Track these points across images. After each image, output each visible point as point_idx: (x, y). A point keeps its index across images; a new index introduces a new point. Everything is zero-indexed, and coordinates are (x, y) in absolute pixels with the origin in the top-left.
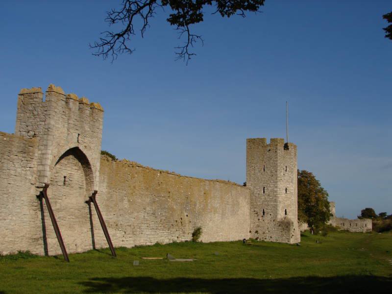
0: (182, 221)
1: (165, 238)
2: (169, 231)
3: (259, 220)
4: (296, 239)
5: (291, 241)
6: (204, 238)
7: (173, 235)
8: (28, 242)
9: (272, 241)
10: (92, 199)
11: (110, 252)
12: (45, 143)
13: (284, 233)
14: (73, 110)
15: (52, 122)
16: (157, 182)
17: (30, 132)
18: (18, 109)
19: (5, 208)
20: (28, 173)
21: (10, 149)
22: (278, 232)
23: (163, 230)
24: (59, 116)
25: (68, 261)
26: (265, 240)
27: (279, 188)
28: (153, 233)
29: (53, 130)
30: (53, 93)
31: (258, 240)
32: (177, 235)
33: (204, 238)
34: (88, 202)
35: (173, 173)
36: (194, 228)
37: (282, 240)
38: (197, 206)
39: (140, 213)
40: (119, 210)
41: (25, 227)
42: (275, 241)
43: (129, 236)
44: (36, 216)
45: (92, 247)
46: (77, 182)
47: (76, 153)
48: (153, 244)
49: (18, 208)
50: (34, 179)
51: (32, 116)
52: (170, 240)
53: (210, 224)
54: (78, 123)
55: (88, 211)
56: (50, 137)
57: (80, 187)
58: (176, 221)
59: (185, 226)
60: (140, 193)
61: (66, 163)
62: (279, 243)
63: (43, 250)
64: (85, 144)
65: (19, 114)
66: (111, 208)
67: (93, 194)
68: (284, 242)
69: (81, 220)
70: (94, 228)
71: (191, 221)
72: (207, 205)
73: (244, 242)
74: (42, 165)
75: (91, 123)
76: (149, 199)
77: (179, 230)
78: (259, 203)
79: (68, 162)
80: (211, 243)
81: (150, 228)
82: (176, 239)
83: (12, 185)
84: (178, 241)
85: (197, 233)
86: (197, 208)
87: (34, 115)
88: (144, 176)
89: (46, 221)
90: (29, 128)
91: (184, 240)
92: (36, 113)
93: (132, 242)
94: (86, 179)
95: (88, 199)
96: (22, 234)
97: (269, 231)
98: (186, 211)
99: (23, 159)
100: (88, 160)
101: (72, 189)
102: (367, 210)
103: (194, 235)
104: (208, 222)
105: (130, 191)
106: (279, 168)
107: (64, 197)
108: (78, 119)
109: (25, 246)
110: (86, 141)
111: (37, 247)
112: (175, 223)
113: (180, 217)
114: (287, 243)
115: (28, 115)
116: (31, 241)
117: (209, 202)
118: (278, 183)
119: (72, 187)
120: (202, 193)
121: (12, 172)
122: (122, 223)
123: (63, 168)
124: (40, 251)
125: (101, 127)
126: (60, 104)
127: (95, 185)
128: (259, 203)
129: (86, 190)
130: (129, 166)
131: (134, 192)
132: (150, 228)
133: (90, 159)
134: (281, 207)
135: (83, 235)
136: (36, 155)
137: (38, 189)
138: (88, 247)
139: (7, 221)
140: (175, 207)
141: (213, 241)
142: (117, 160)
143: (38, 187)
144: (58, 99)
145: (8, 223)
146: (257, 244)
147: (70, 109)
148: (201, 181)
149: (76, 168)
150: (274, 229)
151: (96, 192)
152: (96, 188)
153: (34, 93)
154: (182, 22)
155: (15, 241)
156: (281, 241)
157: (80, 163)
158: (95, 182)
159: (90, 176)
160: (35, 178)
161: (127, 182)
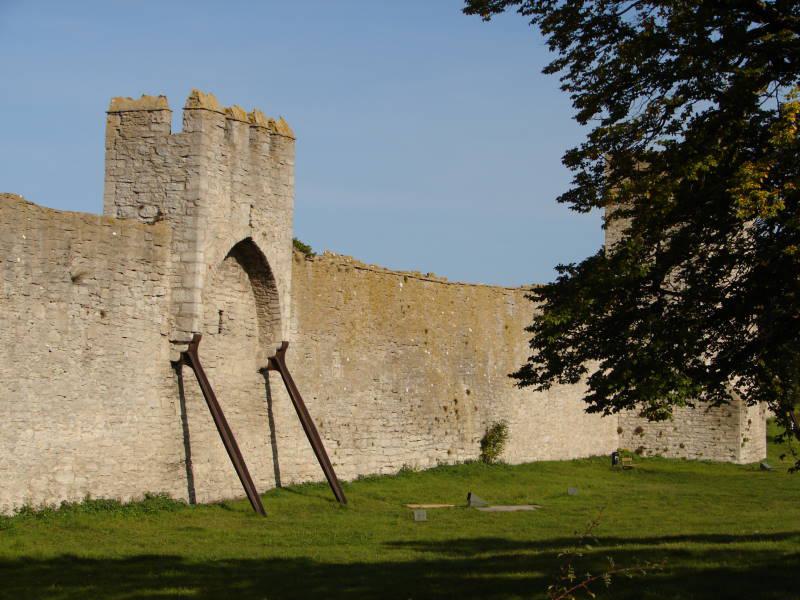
0: (459, 406)
1: (421, 454)
2: (431, 437)
4: (755, 451)
5: (742, 457)
6: (512, 453)
7: (439, 446)
8: (162, 472)
9: (684, 459)
10: (277, 362)
11: (329, 494)
12: (188, 235)
13: (719, 433)
14: (239, 148)
15: (204, 185)
16: (399, 304)
17: (147, 207)
18: (108, 149)
19: (120, 394)
20: (156, 309)
21: (123, 256)
22: (703, 430)
23: (417, 434)
24: (215, 166)
25: (263, 513)
26: (665, 455)
28: (396, 442)
29: (204, 201)
30: (203, 112)
31: (645, 454)
32: (448, 447)
33: (512, 453)
34: (263, 371)
35: (427, 278)
36: (484, 426)
37: (715, 453)
38: (491, 363)
39: (367, 392)
40: (325, 385)
41: (155, 437)
42: (694, 457)
43: (349, 451)
44: (172, 411)
45: (274, 482)
46: (242, 323)
47: (248, 256)
48: (395, 471)
49: (141, 393)
50: (166, 323)
51: (149, 170)
52: (431, 458)
53: (521, 412)
54: (249, 178)
55: (263, 392)
56: (201, 221)
57: (248, 332)
58: (445, 408)
59: (465, 421)
60: (365, 340)
61: (222, 278)
62: (708, 463)
63: (186, 490)
64: (263, 229)
65: (113, 163)
66: (309, 381)
67: (278, 350)
68: (721, 459)
69: (250, 415)
70: (277, 434)
71: (478, 405)
72: (512, 359)
73: (614, 462)
74: (185, 288)
75: (273, 173)
76: (384, 353)
77: (451, 433)
79: (225, 276)
80: (524, 467)
81: (389, 429)
82: (445, 456)
83: (128, 341)
84: (451, 463)
85: (493, 438)
86: (489, 370)
87: (155, 167)
88: (371, 294)
89: (189, 422)
90: (144, 198)
91: (462, 459)
92: (158, 161)
93: (353, 468)
94: (260, 314)
95: (265, 363)
96: (150, 456)
97: (676, 429)
98: (464, 379)
99: (146, 278)
100: (268, 268)
101: (234, 340)
103: (485, 443)
104: (516, 407)
105: (345, 336)
107: (220, 361)
108: (249, 168)
109: (155, 483)
110: (265, 220)
111: (176, 483)
112: (442, 415)
113: (452, 398)
114: (729, 463)
115: (137, 165)
116: (166, 470)
117: (516, 349)
119: (234, 335)
120: (500, 329)
121: (129, 311)
122: (331, 418)
123: (217, 291)
124: (180, 493)
125: (292, 181)
126: (215, 138)
127: (283, 327)
129: (260, 341)
130: (339, 270)
131: (353, 337)
132: (389, 429)
133: (272, 264)
135: (256, 452)
136: (169, 264)
137: (176, 347)
138: (266, 482)
139: (123, 425)
140: (439, 371)
141: (531, 459)
142: (314, 255)
143: (175, 342)
144: (212, 127)
145: (127, 430)
146: (646, 466)
147: (233, 146)
148: (495, 291)
149: (238, 287)
150: (689, 422)
151: (285, 345)
152: (286, 336)
153: (149, 111)
154: (614, 32)
155: (139, 471)
156: (711, 458)
157: (247, 275)
158: (283, 321)
159: (271, 305)
160: (169, 320)
161: (337, 312)
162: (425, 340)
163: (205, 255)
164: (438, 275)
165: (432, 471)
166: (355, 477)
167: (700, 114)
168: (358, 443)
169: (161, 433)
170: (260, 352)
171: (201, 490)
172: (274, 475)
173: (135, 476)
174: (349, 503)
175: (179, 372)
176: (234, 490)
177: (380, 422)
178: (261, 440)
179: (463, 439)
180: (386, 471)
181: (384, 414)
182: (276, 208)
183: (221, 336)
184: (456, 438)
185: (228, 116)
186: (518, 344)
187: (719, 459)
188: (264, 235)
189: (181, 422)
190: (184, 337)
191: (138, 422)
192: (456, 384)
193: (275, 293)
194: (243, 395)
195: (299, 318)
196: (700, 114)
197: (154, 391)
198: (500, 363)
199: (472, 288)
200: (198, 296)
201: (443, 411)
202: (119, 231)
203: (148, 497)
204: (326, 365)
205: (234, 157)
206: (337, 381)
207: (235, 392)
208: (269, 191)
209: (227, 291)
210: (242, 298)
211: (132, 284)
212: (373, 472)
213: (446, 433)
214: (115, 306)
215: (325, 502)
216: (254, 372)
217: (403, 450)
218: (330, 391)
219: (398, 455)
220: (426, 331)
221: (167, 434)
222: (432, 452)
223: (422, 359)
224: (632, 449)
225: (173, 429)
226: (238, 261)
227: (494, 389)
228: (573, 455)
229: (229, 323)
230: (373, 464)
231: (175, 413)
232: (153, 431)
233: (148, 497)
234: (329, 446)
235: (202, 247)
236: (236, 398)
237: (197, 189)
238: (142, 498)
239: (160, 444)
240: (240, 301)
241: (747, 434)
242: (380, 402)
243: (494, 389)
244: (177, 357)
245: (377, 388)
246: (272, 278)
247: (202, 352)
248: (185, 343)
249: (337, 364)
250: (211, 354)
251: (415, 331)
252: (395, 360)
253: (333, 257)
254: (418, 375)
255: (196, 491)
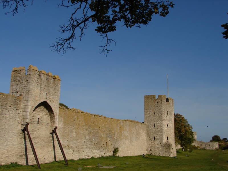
1: (87, 154)
2: (100, 150)
3: (152, 143)
6: (120, 154)
8: (17, 157)
9: (160, 156)
10: (54, 132)
11: (65, 163)
12: (27, 99)
14: (43, 80)
15: (31, 87)
16: (92, 121)
17: (18, 92)
19: (3, 137)
20: (17, 116)
21: (7, 103)
22: (163, 150)
23: (96, 150)
26: (156, 155)
27: (164, 124)
28: (90, 151)
30: (32, 70)
31: (152, 155)
32: (104, 152)
33: (120, 154)
37: (166, 155)
38: (116, 135)
39: (82, 140)
40: (70, 138)
42: (161, 155)
43: (77, 153)
45: (54, 160)
47: (45, 105)
49: (11, 137)
50: (20, 120)
52: (100, 155)
54: (46, 87)
55: (52, 138)
56: (30, 96)
57: (47, 124)
58: (104, 144)
59: (109, 147)
62: (164, 157)
63: (25, 162)
64: (50, 100)
73: (143, 156)
74: (25, 112)
76: (87, 131)
78: (152, 133)
80: (124, 157)
81: (88, 148)
82: (104, 154)
83: (7, 124)
84: (105, 156)
85: (116, 151)
87: (21, 83)
90: (18, 90)
91: (108, 155)
92: (21, 81)
93: (78, 157)
94: (51, 120)
95: (52, 131)
96: (13, 153)
97: (158, 150)
100: (52, 109)
101: (42, 125)
102: (215, 136)
103: (114, 152)
106: (163, 113)
107: (38, 130)
108: (46, 85)
109: (14, 160)
110: (51, 97)
111: (22, 160)
112: (103, 146)
113: (106, 142)
114: (169, 157)
117: (122, 132)
118: (163, 121)
119: (43, 125)
120: (119, 128)
121: (8, 116)
122: (72, 145)
123: (38, 113)
125: (59, 90)
126: (36, 76)
127: (56, 123)
128: (152, 133)
129: (51, 126)
130: (76, 112)
132: (88, 148)
133: (53, 108)
134: (165, 135)
135: (49, 153)
138: (51, 160)
141: (125, 155)
143: (22, 125)
145: (5, 146)
146: (152, 157)
147: (41, 79)
148: (118, 120)
149: (44, 113)
151: (56, 128)
152: (57, 125)
153: (21, 70)
155: (9, 157)
156: (165, 156)
157: (47, 111)
159: (53, 118)
160: (21, 119)
162: (99, 129)
163: (31, 104)
164: (104, 116)
165: (99, 158)
168: (79, 151)
169: (17, 147)
170: (50, 129)
171: (30, 161)
172: (54, 158)
173: (7, 158)
174: (69, 165)
175: (24, 133)
176: (35, 163)
177: (86, 147)
178: (50, 150)
179: (108, 151)
180: (87, 158)
181: (87, 145)
183: (38, 125)
184: (106, 151)
186: (123, 131)
187: (166, 156)
188: (50, 101)
189: (24, 145)
190: (24, 123)
191: (9, 144)
193: (54, 115)
194: (45, 139)
195: (63, 122)
197: (15, 136)
198: (119, 135)
199: (112, 119)
200: (28, 114)
201: (103, 145)
202: (6, 96)
203: (11, 163)
204: (71, 133)
208: (52, 91)
210: (46, 116)
212: (84, 158)
213: (104, 150)
214: (3, 115)
215: (63, 165)
216: (49, 133)
217: (92, 153)
218: (71, 139)
219: (91, 154)
220: (99, 127)
222: (100, 154)
223: (98, 133)
224: (149, 154)
225: (22, 146)
226: (45, 107)
228: (136, 155)
229: (41, 122)
230: (84, 156)
231: (22, 142)
232: (15, 147)
233: (11, 163)
235: (30, 102)
236: (43, 139)
237: (29, 88)
238: (10, 163)
240: (45, 116)
242: (86, 142)
243: (117, 140)
244: (23, 129)
245: (85, 139)
247: (29, 128)
248: (25, 125)
249: (74, 133)
250: (35, 129)
251: (96, 127)
252: (91, 133)
253: (74, 109)
254: (97, 136)
255: (29, 162)
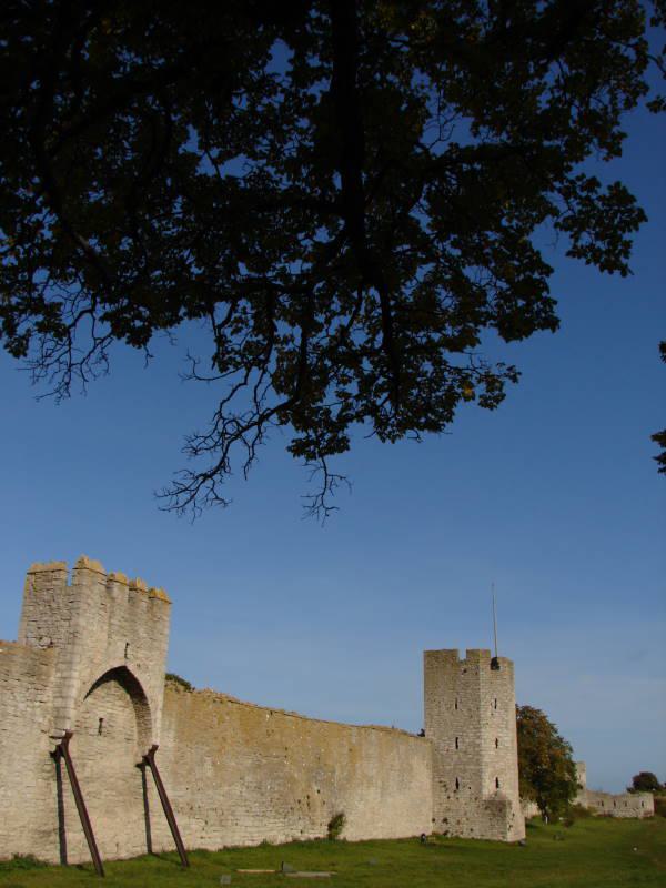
0: (310, 800)
1: (279, 833)
6: (349, 833)
10: (148, 760)
11: (179, 859)
15: (82, 622)
20: (38, 711)
28: (256, 823)
29: (82, 634)
31: (449, 835)
33: (349, 833)
34: (140, 766)
37: (492, 835)
39: (233, 787)
43: (214, 828)
45: (145, 849)
48: (256, 843)
52: (287, 836)
56: (78, 649)
58: (299, 802)
63: (58, 853)
66: (182, 776)
68: (496, 838)
73: (423, 840)
74: (61, 697)
75: (150, 624)
76: (250, 761)
80: (362, 843)
84: (303, 839)
85: (336, 823)
89: (64, 799)
90: (43, 632)
91: (312, 836)
92: (54, 605)
93: (219, 840)
95: (140, 760)
96: (21, 823)
100: (141, 690)
103: (331, 826)
107: (99, 756)
110: (140, 655)
114: (500, 841)
119: (114, 738)
120: (346, 750)
121: (11, 710)
126: (96, 591)
127: (154, 734)
131: (224, 748)
136: (52, 679)
137: (53, 741)
141: (366, 838)
143: (53, 737)
146: (447, 843)
149: (120, 703)
152: (156, 741)
158: (154, 729)
160: (50, 721)
166: (221, 847)
167: (290, 68)
168: (223, 823)
175: (57, 761)
182: (150, 649)
183: (100, 737)
185: (152, 595)
188: (139, 666)
192: (309, 786)
194: (120, 782)
196: (290, 68)
200: (71, 704)
203: (16, 857)
205: (112, 607)
206: (208, 778)
207: (112, 780)
209: (109, 704)
211: (15, 690)
215: (174, 865)
218: (201, 784)
221: (40, 808)
222: (287, 832)
224: (441, 832)
225: (48, 804)
227: (340, 790)
228: (399, 835)
229: (110, 729)
231: (51, 791)
234: (180, 821)
236: (112, 784)
237: (77, 625)
239: (34, 815)
241: (511, 823)
243: (340, 790)
244: (54, 749)
246: (145, 698)
254: (278, 777)
255: (68, 854)
